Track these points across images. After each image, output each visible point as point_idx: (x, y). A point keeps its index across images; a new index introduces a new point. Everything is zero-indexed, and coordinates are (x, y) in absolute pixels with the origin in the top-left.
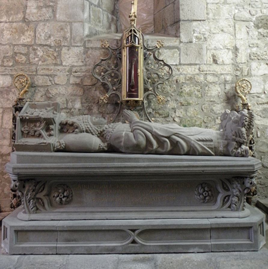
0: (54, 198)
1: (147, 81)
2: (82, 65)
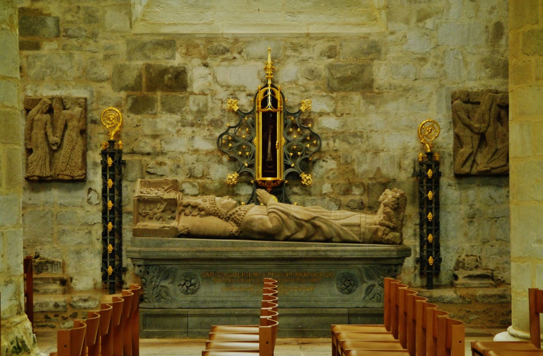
1: (289, 156)
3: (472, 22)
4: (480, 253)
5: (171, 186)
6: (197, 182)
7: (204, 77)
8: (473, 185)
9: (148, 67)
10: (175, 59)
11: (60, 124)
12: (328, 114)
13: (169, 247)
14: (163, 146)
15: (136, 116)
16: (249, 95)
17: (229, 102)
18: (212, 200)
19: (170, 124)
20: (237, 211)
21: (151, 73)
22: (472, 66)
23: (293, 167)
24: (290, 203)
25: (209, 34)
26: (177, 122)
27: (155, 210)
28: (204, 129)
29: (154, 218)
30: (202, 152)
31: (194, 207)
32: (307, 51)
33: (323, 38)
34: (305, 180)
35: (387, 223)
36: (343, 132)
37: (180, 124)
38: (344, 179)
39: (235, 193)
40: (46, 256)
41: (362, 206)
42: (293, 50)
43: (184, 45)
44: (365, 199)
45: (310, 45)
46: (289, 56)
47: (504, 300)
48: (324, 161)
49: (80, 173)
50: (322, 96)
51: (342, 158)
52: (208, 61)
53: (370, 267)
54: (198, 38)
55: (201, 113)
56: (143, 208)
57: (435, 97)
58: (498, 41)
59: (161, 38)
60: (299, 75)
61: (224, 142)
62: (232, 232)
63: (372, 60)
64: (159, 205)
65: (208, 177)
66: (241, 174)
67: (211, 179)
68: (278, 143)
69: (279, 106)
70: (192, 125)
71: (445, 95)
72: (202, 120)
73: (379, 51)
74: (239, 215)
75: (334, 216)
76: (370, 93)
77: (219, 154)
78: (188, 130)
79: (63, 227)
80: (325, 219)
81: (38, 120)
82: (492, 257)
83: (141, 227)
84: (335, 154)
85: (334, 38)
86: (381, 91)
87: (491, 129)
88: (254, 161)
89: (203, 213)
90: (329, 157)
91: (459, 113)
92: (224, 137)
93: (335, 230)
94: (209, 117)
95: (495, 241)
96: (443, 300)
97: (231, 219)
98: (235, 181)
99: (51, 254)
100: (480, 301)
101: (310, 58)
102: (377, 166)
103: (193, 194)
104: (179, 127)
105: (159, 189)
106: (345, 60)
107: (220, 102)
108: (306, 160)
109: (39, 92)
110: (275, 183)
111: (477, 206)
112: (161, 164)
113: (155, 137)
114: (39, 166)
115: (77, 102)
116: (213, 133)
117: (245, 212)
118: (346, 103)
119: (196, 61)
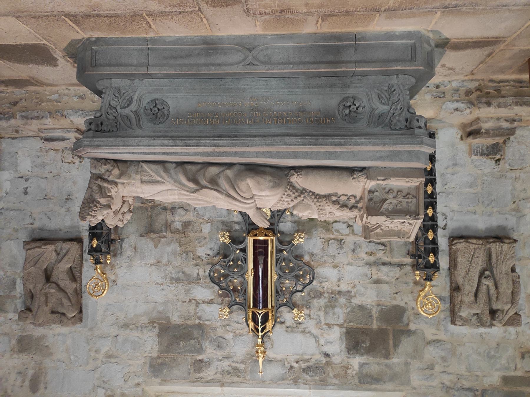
0: (363, 105)
1: (242, 261)
2: (241, 59)
3: (59, 393)
4: (62, 166)
5: (372, 232)
6: (334, 235)
7: (328, 342)
8: (66, 230)
9: (387, 356)
10: (359, 363)
11: (482, 295)
12: (204, 302)
13: (381, 151)
14: (370, 272)
15: (398, 304)
16: (282, 323)
17: (302, 318)
18: (322, 214)
19: (362, 295)
20: (292, 200)
21: (384, 348)
22: (61, 349)
23: (238, 249)
24: (240, 212)
25: (324, 389)
26: (355, 296)
27: (394, 201)
28: (328, 288)
29: (396, 192)
30: (329, 265)
31: (344, 206)
32: (223, 367)
33: (207, 382)
34: (226, 236)
35: (105, 185)
36: (190, 283)
37: (353, 294)
38: (189, 236)
39: (296, 224)
40: (489, 161)
41: (173, 211)
42: (238, 369)
43: (350, 378)
44: (170, 217)
45: (221, 374)
46: (241, 362)
47: (23, 114)
48: (209, 255)
49: (459, 246)
50: (209, 320)
51: (192, 258)
52: (324, 360)
53: (126, 130)
54: (335, 384)
55: (331, 305)
56: (410, 205)
57: (99, 318)
58: (35, 373)
59: (373, 386)
60: (232, 342)
61: (308, 276)
62: (298, 175)
63: (159, 357)
64: (391, 208)
65: (324, 240)
66: (290, 242)
67: (320, 238)
68: (251, 275)
69: (251, 314)
70: (340, 293)
71: (89, 320)
72: (330, 297)
73: (151, 366)
74: (289, 195)
75: (174, 195)
76: (162, 323)
77: (312, 263)
78: (344, 287)
79: (472, 190)
80: (184, 190)
81: (507, 303)
82: (51, 162)
83: (415, 180)
84: (198, 261)
85: (197, 381)
86: (152, 324)
87: (39, 287)
88: (277, 256)
89: (334, 198)
90: (203, 258)
91: (69, 304)
92: (307, 281)
93: (171, 177)
94: (322, 301)
95: (48, 176)
96: (83, 113)
97: (299, 191)
98: (296, 236)
99: (483, 164)
100: (47, 112)
101: (221, 360)
102: (157, 250)
103: (338, 223)
104: (353, 291)
105: (387, 229)
106: (185, 357)
107: (312, 316)
108: (225, 256)
109: (502, 331)
110: (255, 233)
111: (63, 210)
112: (371, 254)
113: (378, 282)
114: (503, 254)
115: (464, 321)
116: (319, 285)
117: (282, 199)
118: (186, 313)
119: (336, 359)
